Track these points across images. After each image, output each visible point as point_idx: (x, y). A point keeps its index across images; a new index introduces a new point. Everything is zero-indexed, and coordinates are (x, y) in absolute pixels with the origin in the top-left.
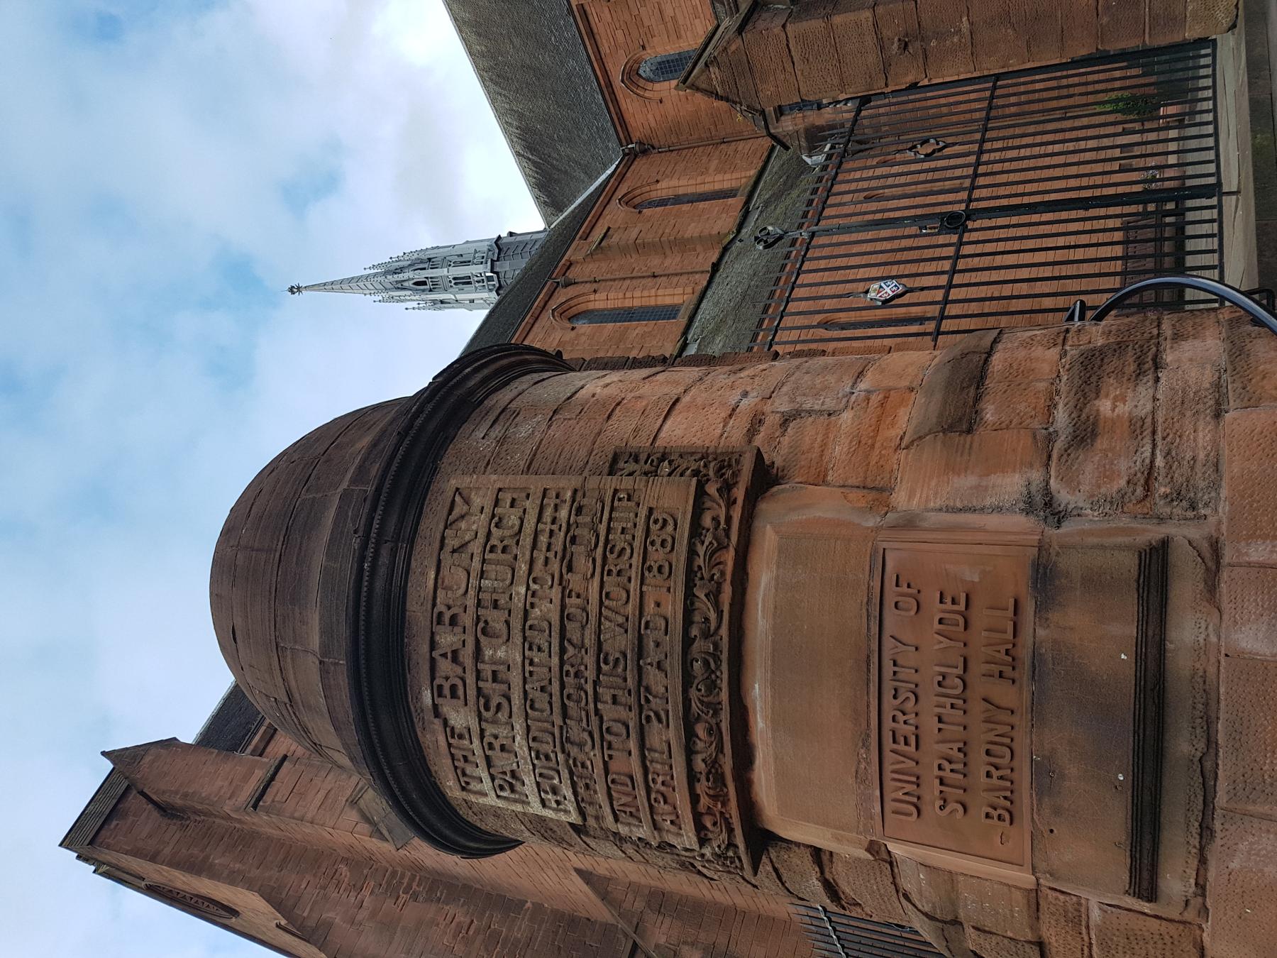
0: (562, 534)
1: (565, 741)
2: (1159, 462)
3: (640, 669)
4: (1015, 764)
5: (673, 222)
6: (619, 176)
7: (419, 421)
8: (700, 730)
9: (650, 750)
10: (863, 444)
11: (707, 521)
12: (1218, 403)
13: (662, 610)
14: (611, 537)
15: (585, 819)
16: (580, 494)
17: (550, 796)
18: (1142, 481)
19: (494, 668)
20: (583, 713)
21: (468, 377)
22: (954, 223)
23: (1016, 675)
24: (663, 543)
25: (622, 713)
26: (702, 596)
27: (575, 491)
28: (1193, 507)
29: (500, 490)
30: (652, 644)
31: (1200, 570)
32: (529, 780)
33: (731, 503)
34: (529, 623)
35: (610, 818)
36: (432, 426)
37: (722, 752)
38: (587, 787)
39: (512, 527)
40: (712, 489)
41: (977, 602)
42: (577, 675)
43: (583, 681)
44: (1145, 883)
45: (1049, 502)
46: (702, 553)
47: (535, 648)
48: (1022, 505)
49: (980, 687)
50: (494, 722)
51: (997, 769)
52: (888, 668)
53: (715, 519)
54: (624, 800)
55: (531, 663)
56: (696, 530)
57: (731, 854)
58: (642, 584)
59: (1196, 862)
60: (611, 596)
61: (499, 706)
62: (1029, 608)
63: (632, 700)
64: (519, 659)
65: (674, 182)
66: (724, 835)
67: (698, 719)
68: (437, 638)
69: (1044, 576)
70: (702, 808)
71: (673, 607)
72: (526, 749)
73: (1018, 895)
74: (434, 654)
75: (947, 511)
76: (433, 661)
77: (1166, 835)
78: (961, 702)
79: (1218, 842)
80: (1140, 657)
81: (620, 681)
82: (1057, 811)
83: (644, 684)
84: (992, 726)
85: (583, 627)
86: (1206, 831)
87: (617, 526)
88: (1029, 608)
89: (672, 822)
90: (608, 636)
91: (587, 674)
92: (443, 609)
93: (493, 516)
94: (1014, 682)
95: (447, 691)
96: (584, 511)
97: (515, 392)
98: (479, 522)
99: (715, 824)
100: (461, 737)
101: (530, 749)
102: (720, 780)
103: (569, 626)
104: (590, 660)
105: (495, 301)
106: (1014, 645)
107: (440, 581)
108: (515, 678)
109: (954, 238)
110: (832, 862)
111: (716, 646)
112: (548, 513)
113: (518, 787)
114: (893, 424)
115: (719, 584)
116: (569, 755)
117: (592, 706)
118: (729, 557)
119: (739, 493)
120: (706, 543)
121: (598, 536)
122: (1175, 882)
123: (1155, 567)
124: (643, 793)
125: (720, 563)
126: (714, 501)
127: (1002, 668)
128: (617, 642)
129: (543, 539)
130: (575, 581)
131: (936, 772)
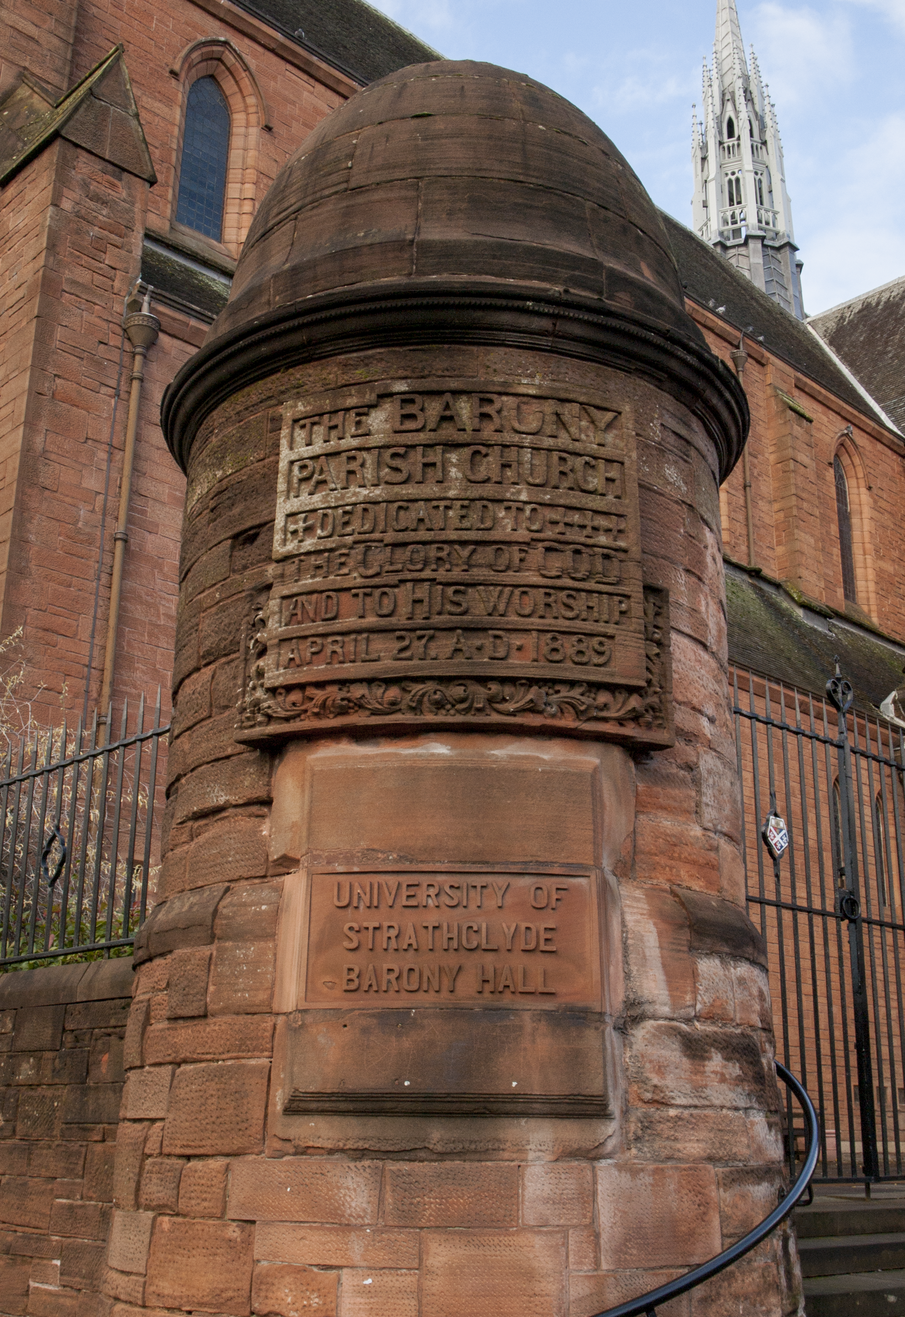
0: (583, 539)
1: (366, 544)
2: (672, 1112)
3: (452, 629)
4: (404, 994)
5: (817, 512)
6: (878, 435)
7: (681, 353)
8: (393, 692)
9: (368, 639)
10: (674, 845)
11: (603, 697)
12: (720, 1159)
13: (514, 653)
14: (583, 594)
15: (278, 561)
16: (621, 555)
17: (301, 524)
18: (656, 1098)
19: (439, 464)
20: (399, 566)
21: (721, 395)
22: (848, 908)
23: (487, 994)
24: (580, 652)
25: (404, 610)
26: (530, 696)
27: (625, 551)
28: (638, 1139)
29: (622, 463)
30: (478, 643)
31: (589, 1145)
32: (317, 500)
33: (621, 722)
34: (490, 505)
35: (286, 592)
36: (674, 365)
37: (373, 714)
38: (319, 567)
39: (586, 481)
40: (634, 702)
41: (547, 961)
42: (439, 559)
43: (434, 567)
44: (297, 1107)
45: (637, 1020)
46: (571, 694)
47: (464, 512)
48: (632, 996)
49: (472, 962)
50: (379, 464)
51: (397, 978)
52: (479, 881)
53: (605, 706)
54: (310, 608)
55: (447, 508)
56: (596, 687)
57: (260, 718)
58: (539, 631)
59: (330, 1146)
60: (525, 598)
61: (397, 470)
62: (548, 1005)
63: (419, 621)
64: (452, 493)
65: (867, 512)
66: (283, 714)
67: (404, 690)
68: (464, 398)
69: (576, 1018)
70: (310, 691)
71: (520, 664)
72: (353, 499)
73: (262, 996)
74: (448, 394)
75: (623, 932)
76: (439, 393)
77: (353, 1121)
78: (456, 946)
79: (352, 1165)
80: (514, 1097)
81: (437, 608)
82: (365, 1031)
83: (438, 634)
84: (437, 975)
85: (490, 566)
86: (360, 1154)
87: (594, 601)
88: (548, 1005)
89: (292, 659)
90: (483, 594)
91: (442, 571)
92: (497, 405)
93: (595, 458)
94: (480, 992)
95: (410, 409)
96: (606, 562)
97: (705, 452)
98: (590, 441)
99: (294, 704)
100: (358, 423)
101: (355, 504)
102: (343, 711)
103: (490, 550)
104: (457, 574)
105: (705, 239)
106: (513, 993)
107: (525, 399)
108: (431, 489)
109: (830, 908)
110: (250, 816)
111: (479, 710)
112: (602, 522)
113: (306, 488)
114: (691, 876)
115: (540, 712)
116: (351, 548)
117: (409, 576)
118: (568, 722)
119: (630, 730)
120: (583, 699)
121: (583, 580)
122: (319, 1130)
123: (588, 1108)
124: (321, 630)
125: (562, 711)
126: (624, 703)
127: (492, 982)
128: (478, 604)
129: (576, 518)
130: (536, 555)
131: (386, 924)
